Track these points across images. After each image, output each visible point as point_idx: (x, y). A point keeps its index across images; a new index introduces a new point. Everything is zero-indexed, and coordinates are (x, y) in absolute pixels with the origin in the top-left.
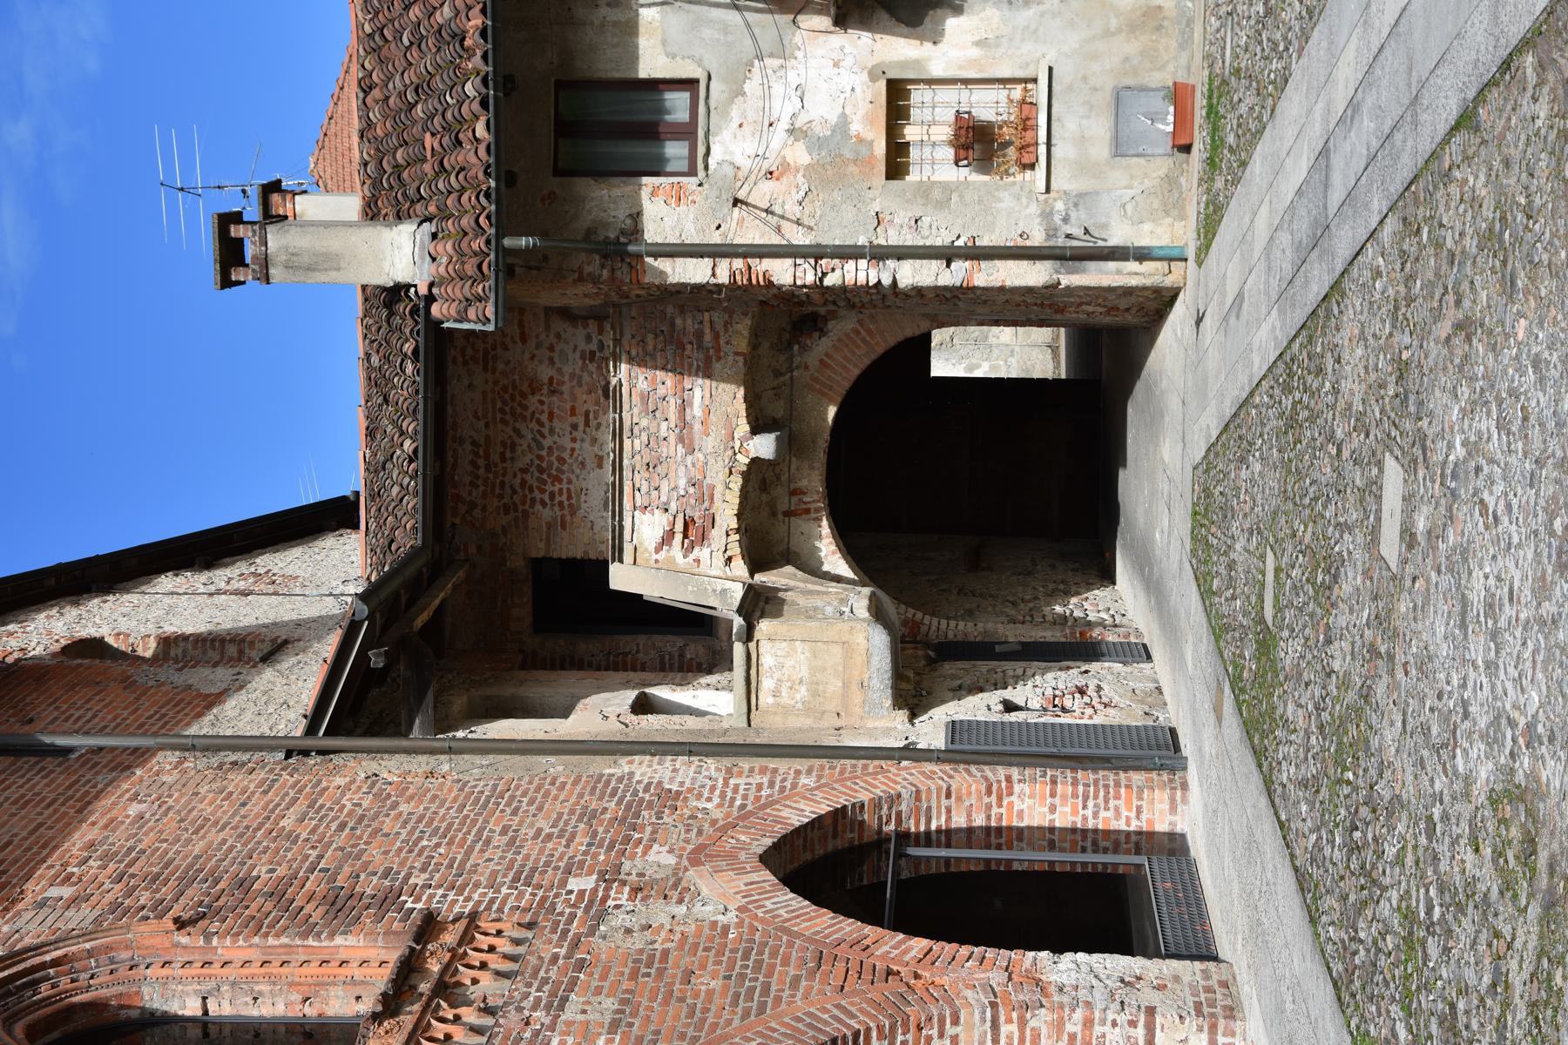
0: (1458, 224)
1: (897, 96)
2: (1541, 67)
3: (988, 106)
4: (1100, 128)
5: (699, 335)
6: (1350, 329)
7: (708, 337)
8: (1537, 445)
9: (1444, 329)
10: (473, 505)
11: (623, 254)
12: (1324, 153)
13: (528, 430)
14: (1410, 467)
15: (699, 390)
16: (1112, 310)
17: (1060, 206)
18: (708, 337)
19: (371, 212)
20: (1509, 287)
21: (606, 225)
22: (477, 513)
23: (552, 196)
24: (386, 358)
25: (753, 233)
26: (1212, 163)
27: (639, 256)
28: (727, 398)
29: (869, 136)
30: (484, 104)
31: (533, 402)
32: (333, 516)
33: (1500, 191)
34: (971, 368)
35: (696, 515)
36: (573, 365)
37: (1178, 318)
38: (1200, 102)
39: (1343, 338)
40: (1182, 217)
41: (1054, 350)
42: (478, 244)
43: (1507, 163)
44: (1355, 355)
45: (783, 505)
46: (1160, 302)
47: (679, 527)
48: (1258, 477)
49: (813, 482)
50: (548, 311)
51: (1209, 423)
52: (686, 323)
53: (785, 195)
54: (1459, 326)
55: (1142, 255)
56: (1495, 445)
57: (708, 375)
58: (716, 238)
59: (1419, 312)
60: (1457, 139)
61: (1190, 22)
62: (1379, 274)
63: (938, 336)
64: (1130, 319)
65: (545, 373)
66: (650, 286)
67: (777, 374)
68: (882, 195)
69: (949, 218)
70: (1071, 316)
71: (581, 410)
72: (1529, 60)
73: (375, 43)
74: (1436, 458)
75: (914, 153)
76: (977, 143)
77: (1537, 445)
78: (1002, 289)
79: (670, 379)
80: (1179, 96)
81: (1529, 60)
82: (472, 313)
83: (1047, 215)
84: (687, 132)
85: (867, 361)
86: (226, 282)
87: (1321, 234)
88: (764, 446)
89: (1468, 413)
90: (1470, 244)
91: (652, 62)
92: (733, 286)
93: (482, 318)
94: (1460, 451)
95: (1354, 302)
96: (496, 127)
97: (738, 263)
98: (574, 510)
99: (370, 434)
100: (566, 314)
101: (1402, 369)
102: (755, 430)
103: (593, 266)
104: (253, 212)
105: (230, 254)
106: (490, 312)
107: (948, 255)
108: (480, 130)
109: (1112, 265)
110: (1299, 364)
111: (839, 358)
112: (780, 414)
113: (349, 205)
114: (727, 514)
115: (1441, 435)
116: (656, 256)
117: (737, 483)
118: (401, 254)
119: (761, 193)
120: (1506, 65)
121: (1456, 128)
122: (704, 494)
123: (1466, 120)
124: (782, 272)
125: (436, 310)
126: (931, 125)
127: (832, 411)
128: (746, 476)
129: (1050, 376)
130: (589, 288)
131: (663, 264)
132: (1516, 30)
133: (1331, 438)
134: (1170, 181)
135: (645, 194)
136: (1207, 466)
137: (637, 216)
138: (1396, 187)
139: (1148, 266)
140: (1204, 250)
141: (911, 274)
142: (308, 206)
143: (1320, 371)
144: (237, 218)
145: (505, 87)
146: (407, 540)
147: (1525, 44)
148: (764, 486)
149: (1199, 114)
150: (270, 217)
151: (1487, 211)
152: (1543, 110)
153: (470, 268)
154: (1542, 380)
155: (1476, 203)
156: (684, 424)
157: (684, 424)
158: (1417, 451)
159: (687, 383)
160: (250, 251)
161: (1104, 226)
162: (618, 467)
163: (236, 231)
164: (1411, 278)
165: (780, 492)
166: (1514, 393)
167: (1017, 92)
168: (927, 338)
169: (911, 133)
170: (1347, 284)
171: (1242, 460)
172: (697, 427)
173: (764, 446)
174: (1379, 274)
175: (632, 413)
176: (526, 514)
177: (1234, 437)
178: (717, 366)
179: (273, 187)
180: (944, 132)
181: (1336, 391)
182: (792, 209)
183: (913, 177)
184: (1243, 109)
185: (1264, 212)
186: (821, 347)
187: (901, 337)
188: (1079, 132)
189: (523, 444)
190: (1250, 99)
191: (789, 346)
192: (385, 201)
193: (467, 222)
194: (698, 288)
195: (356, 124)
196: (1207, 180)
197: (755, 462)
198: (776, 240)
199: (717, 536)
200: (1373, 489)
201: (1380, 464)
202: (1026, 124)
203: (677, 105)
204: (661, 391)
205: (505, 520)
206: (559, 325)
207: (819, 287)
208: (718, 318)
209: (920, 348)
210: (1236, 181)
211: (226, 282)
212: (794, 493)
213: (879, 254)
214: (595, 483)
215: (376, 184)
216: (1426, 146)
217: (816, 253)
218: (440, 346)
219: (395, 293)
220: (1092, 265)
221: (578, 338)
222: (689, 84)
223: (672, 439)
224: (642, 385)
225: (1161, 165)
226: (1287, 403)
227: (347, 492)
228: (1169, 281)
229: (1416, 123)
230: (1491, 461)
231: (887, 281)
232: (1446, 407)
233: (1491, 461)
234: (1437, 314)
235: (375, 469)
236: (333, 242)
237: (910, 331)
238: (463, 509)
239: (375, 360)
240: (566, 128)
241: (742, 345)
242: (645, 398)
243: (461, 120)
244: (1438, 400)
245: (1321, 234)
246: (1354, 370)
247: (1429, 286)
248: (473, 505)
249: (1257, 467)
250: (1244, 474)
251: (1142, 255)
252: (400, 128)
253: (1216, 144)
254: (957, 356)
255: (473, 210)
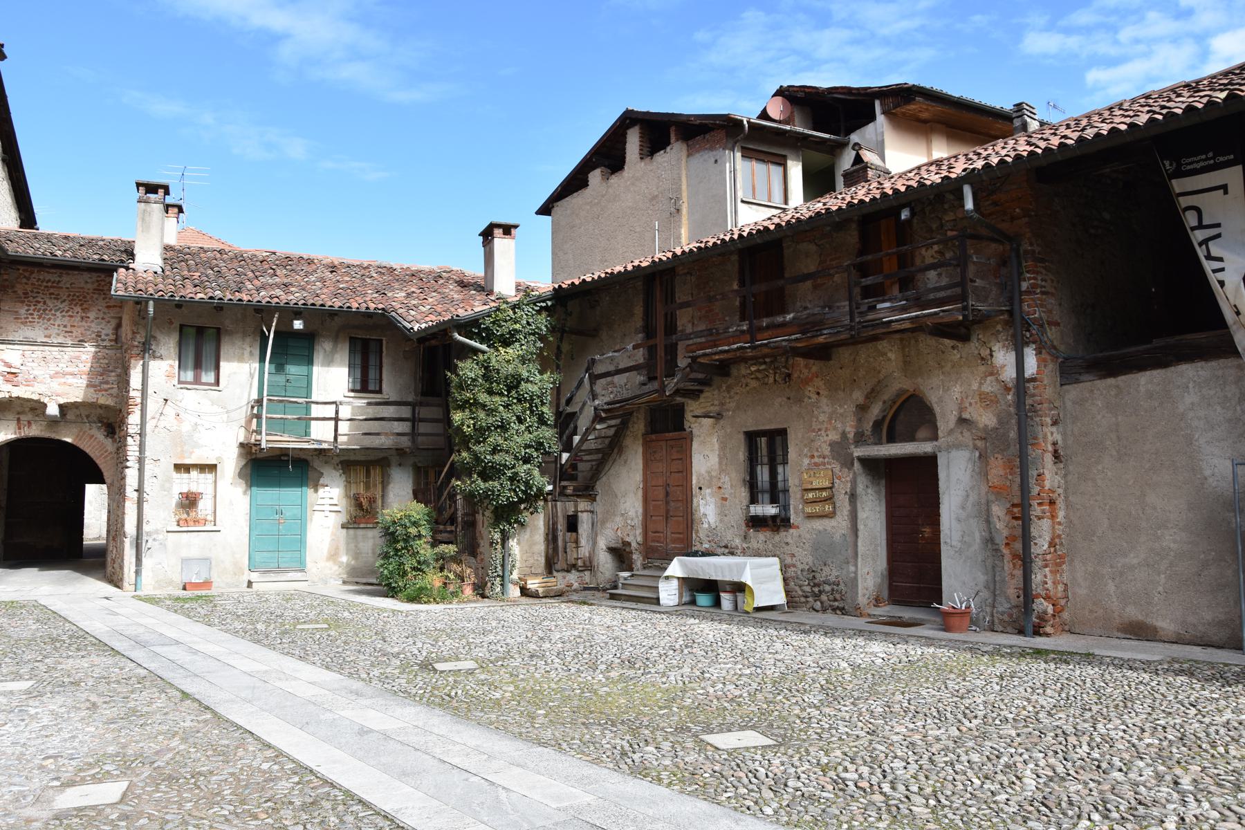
0: (140, 700)
1: (212, 468)
2: (205, 721)
3: (204, 506)
4: (194, 552)
5: (107, 383)
6: (96, 660)
7: (106, 386)
8: (33, 743)
9: (93, 698)
10: (28, 279)
11: (144, 351)
12: (177, 643)
13: (65, 306)
14: (28, 692)
15: (82, 382)
16: (114, 561)
17: (161, 537)
18: (106, 386)
19: (167, 248)
20: (112, 721)
21: (157, 345)
22: (24, 280)
23: (171, 323)
24: (101, 248)
25: (153, 406)
26: (178, 599)
27: (143, 358)
28: (77, 394)
29: (193, 456)
30: (211, 298)
31: (78, 309)
32: (27, 218)
33: (154, 713)
34: (90, 502)
35: (19, 378)
36: (95, 327)
37: (109, 589)
38: (204, 593)
39: (94, 658)
40: (154, 588)
41: (98, 538)
42: (151, 291)
43: (166, 714)
44: (85, 663)
45: (23, 417)
46: (116, 582)
47: (13, 370)
48: (29, 627)
49: (35, 431)
50: (120, 318)
51: (57, 605)
52: (112, 377)
53: (169, 420)
54: (94, 704)
55: (138, 573)
56: (35, 726)
57: (87, 386)
58: (150, 391)
59: (102, 687)
60: (178, 693)
61: (237, 586)
62: (121, 669)
63: (104, 487)
64: (109, 569)
65: (92, 315)
66: (129, 361)
67: (88, 417)
68: (167, 463)
69: (152, 478)
70: (112, 543)
71: (73, 329)
72: (209, 716)
73: (240, 258)
74: (31, 702)
75: (186, 476)
76: (189, 501)
77: (33, 743)
78: (124, 513)
79: (87, 369)
80: (207, 584)
81: (209, 716)
82: (120, 284)
83: (157, 532)
84: (197, 381)
85: (92, 456)
86: (139, 185)
87: (142, 644)
88: (53, 410)
89: (52, 712)
90: (132, 704)
91: (227, 367)
92: (129, 398)
93: (117, 289)
94: (32, 711)
95: (110, 661)
96: (201, 303)
97: (139, 400)
98: (24, 323)
99: (66, 238)
100: (119, 326)
101: (76, 684)
102: (60, 406)
103: (140, 338)
104: (169, 200)
105: (151, 188)
106: (120, 293)
107: (140, 490)
108: (200, 295)
109: (134, 560)
110: (82, 640)
111: (93, 443)
112: (68, 417)
113: (172, 240)
114: (17, 392)
115: (43, 703)
116: (143, 365)
117: (35, 397)
118: (148, 259)
119: (170, 410)
120: (207, 708)
121: (183, 692)
122: (28, 383)
123: (185, 695)
124: (134, 419)
125: (122, 270)
126: (196, 482)
127: (69, 440)
128: (38, 402)
129: (85, 536)
130: (130, 336)
131: (139, 368)
132: (221, 710)
133: (45, 657)
134: (170, 583)
135: (171, 362)
136: (37, 605)
137: (161, 358)
138: (160, 673)
139: (133, 575)
140: (140, 598)
141: (131, 476)
142: (171, 223)
143: (78, 650)
144: (167, 192)
145: (219, 308)
146: (11, 248)
147: (215, 713)
148: (33, 409)
149: (199, 593)
150: (167, 207)
151: (146, 709)
152: (188, 724)
153: (140, 286)
154: (65, 740)
155: (150, 704)
156: (65, 374)
157: (65, 374)
158: (35, 694)
159: (84, 377)
160: (152, 196)
161: (151, 556)
162: (44, 344)
163: (161, 192)
164: (118, 682)
165: (30, 417)
166: (60, 729)
167: (210, 518)
168: (102, 481)
169: (194, 474)
170: (118, 657)
171: (38, 621)
172: (63, 380)
173: (53, 410)
174: (121, 669)
175: (71, 352)
176: (23, 302)
177: (49, 616)
178: (92, 390)
179: (181, 210)
180: (194, 489)
181: (68, 657)
182: (161, 424)
183: (175, 475)
184: (199, 609)
185: (154, 621)
186: (100, 435)
187: (101, 467)
188: (193, 544)
189: (58, 303)
190: (203, 612)
191: (100, 422)
192: (173, 256)
193: (161, 287)
194: (128, 383)
195: (206, 246)
196: (170, 597)
197: (45, 405)
198: (148, 417)
199: (8, 387)
200: (18, 677)
201: (31, 679)
202: (196, 522)
203: (209, 377)
204: (81, 365)
205: (20, 292)
206: (114, 323)
207: (127, 435)
208: (115, 391)
209: (98, 479)
210: (168, 609)
211: (139, 185)
212: (29, 423)
213: (141, 461)
214: (37, 334)
215: (180, 251)
216: (175, 682)
217: (142, 434)
218: (105, 271)
219: (131, 255)
220: (134, 552)
221: (108, 330)
222: (217, 383)
223: (58, 369)
224: (84, 357)
225: (178, 579)
226: (64, 638)
227: (39, 225)
228: (126, 584)
229: (186, 677)
230: (26, 725)
231: (128, 464)
232: (56, 703)
233: (26, 725)
234: (100, 695)
235: (49, 238)
236: (155, 231)
237: (106, 475)
238: (27, 274)
239: (101, 243)
240: (200, 331)
241: (101, 401)
242: (78, 358)
243: (205, 288)
244: (60, 700)
245: (142, 644)
246: (76, 664)
247: (115, 690)
248: (28, 279)
249: (34, 627)
250: (31, 622)
251: (138, 573)
252: (203, 264)
253: (185, 600)
254: (95, 495)
255: (166, 289)
